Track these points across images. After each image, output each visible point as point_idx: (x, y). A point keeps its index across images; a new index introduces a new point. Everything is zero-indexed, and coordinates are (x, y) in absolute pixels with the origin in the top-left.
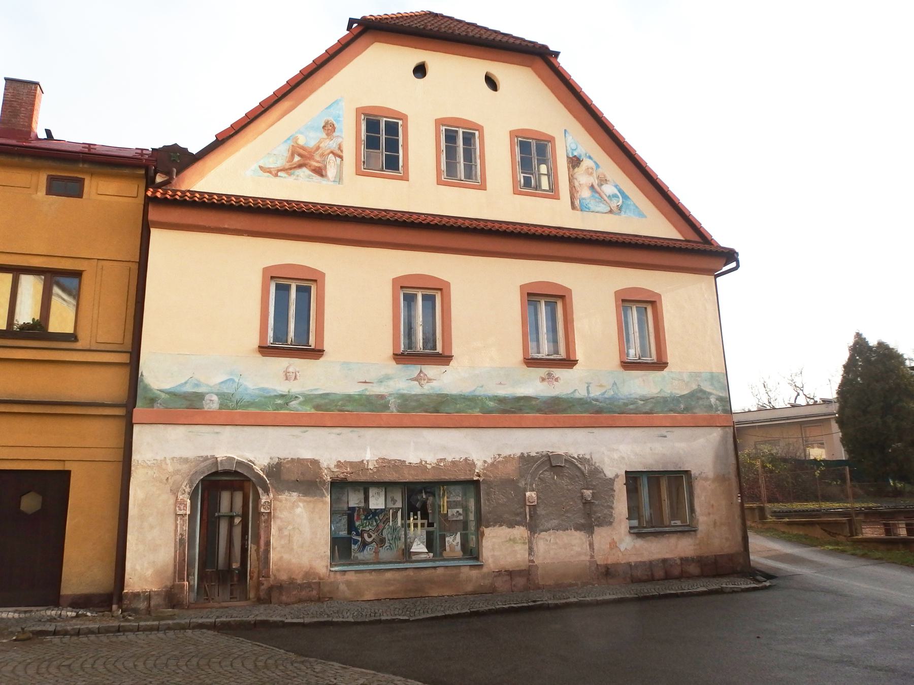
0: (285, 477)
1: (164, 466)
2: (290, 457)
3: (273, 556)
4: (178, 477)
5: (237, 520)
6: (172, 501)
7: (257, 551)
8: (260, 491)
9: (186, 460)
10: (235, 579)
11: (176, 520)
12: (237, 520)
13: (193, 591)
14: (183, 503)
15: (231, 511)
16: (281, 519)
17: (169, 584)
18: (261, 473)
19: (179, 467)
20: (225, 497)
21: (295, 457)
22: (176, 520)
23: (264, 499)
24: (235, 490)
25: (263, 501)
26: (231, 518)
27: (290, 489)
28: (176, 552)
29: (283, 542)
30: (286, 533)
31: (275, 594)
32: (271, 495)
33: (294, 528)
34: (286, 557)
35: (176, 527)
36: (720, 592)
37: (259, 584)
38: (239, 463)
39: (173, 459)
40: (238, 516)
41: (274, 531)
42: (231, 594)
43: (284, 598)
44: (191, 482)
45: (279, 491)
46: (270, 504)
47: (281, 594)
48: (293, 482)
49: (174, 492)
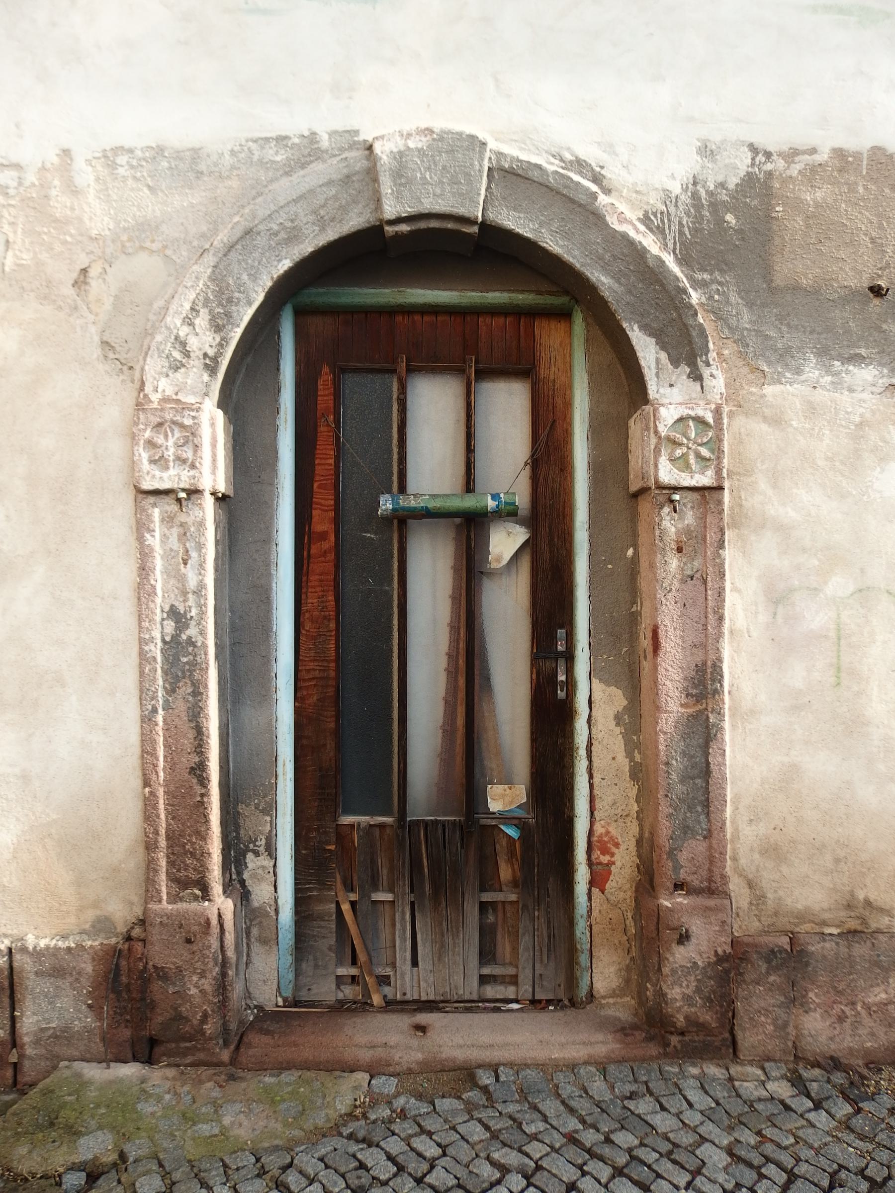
0: (794, 266)
1: (60, 203)
2: (826, 141)
3: (743, 760)
4: (144, 268)
5: (505, 543)
6: (114, 411)
7: (635, 720)
8: (648, 352)
9: (189, 165)
10: (505, 872)
11: (141, 527)
12: (505, 543)
13: (270, 940)
14: (174, 420)
15: (469, 486)
16: (783, 529)
17: (121, 911)
18: (651, 243)
19: (150, 206)
20: (433, 406)
21: (859, 142)
22: (141, 527)
23: (671, 397)
24: (484, 374)
25: (668, 415)
26: (471, 527)
27: (837, 349)
28: (147, 719)
29: (797, 675)
30: (816, 618)
31: (758, 1001)
32: (717, 381)
33: (863, 592)
34: (821, 766)
35: (144, 571)
36: (590, 744)
37: (650, 937)
38: (512, 177)
39: (109, 158)
40: (508, 513)
41: (741, 604)
42: (487, 954)
43: (817, 1028)
44: (221, 299)
45: (768, 356)
46: (711, 430)
47: (795, 1000)
48: (851, 296)
49: (121, 356)
